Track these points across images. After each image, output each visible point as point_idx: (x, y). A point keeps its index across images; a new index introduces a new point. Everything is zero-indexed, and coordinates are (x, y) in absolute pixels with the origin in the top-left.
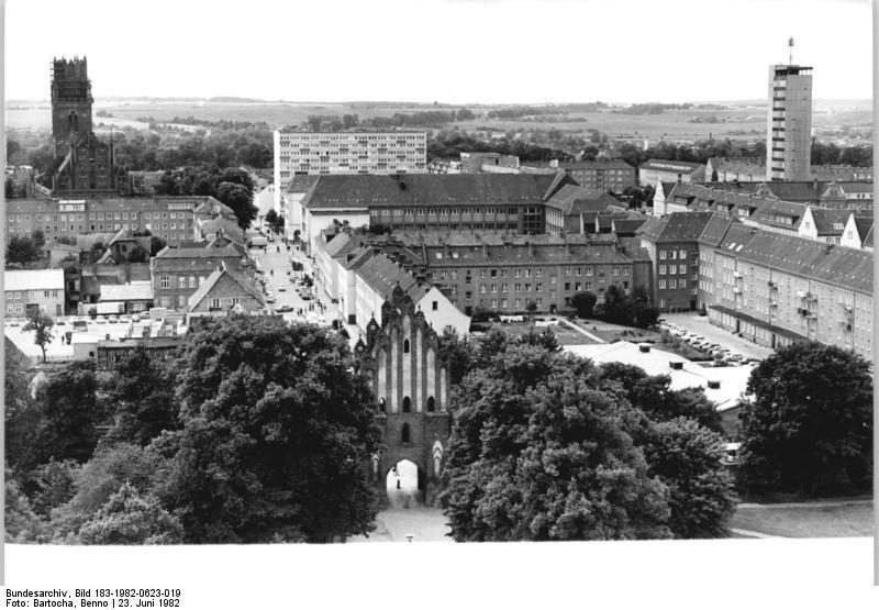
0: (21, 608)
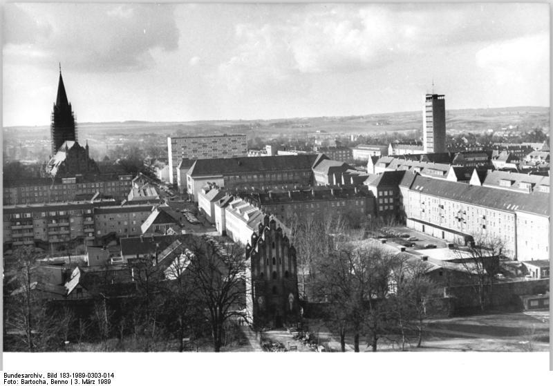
0: (13, 385)
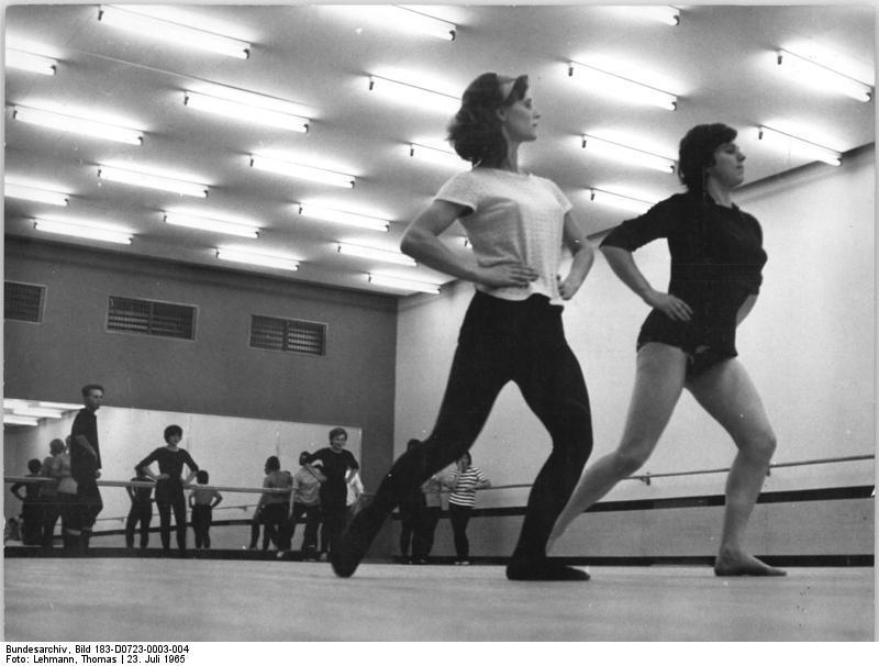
0: (21, 664)
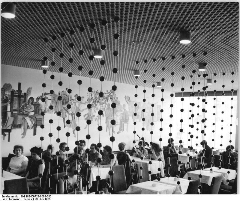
0: (6, 200)
